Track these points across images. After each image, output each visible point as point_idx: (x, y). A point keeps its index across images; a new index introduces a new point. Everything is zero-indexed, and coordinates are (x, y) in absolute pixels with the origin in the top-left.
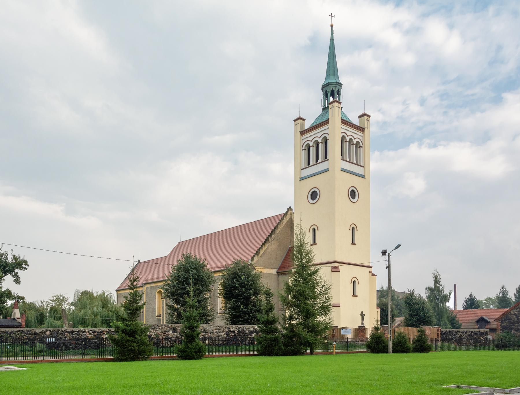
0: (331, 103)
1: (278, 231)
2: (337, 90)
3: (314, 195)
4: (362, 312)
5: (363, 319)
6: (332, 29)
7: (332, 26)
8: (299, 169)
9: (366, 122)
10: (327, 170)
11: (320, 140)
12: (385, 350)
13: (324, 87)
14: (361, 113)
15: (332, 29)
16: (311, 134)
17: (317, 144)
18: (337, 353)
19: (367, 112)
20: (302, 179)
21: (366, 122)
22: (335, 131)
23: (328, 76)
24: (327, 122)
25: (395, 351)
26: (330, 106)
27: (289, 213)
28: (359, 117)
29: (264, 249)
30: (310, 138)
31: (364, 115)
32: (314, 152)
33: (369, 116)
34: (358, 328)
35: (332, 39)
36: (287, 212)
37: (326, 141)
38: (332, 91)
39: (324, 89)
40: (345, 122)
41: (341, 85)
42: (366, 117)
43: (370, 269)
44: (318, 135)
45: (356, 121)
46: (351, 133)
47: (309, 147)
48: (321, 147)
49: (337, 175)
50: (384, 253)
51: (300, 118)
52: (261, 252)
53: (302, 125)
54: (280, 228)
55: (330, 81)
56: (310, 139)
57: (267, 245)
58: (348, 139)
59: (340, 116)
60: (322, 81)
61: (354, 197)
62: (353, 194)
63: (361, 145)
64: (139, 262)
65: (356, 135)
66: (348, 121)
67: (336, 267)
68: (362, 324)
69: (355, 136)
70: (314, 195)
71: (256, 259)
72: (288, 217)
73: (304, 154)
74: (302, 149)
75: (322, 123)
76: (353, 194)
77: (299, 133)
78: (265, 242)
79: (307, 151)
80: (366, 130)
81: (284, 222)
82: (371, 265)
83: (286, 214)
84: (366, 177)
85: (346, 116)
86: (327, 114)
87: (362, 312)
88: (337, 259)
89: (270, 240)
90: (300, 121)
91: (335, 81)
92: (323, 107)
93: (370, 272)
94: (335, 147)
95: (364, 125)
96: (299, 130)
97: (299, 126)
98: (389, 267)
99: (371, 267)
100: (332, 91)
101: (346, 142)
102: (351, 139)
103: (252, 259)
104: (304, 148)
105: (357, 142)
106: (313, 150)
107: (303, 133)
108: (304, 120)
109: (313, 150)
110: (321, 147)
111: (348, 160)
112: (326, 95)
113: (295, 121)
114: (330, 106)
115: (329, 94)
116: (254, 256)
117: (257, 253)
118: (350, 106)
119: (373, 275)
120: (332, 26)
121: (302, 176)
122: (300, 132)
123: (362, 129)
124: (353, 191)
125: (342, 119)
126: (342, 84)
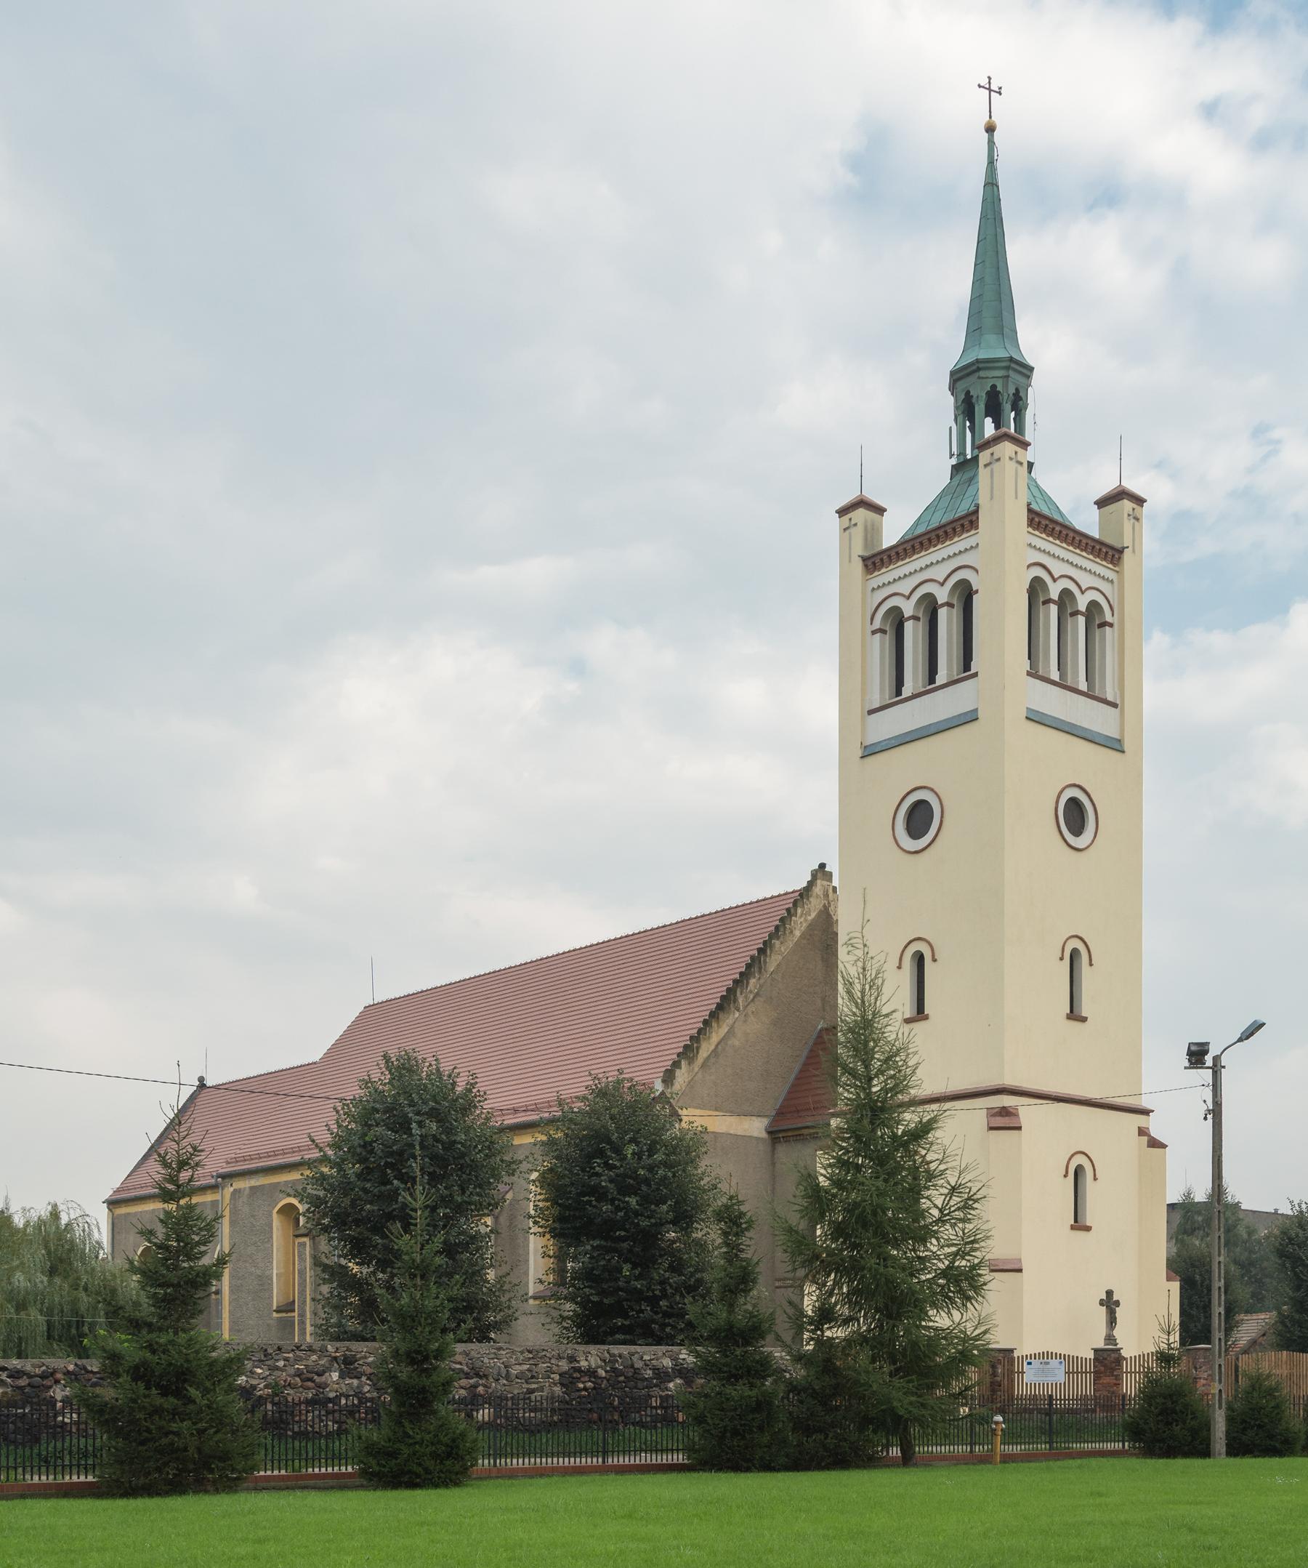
1: (773, 962)
2: (1012, 391)
3: (919, 818)
4: (1110, 1293)
5: (1112, 1321)
6: (991, 143)
7: (990, 129)
9: (1128, 525)
10: (971, 718)
12: (1198, 1447)
13: (958, 377)
14: (1107, 486)
15: (991, 143)
17: (930, 607)
18: (1007, 1459)
20: (870, 751)
21: (1128, 525)
22: (1004, 560)
23: (975, 330)
24: (969, 521)
25: (1237, 1448)
26: (984, 457)
27: (818, 890)
28: (1101, 503)
29: (716, 1035)
30: (904, 584)
31: (1120, 495)
32: (916, 635)
33: (1140, 501)
34: (1091, 1355)
35: (991, 184)
36: (811, 884)
37: (965, 595)
38: (990, 393)
39: (961, 385)
40: (1044, 522)
42: (1127, 505)
43: (1140, 1120)
44: (933, 571)
45: (1088, 521)
47: (897, 621)
48: (947, 622)
50: (1197, 1055)
51: (862, 503)
52: (705, 1049)
53: (872, 533)
54: (782, 949)
56: (905, 587)
57: (730, 1021)
59: (1024, 498)
61: (1077, 829)
62: (1075, 815)
63: (1108, 618)
64: (202, 1085)
67: (1005, 1112)
68: (1110, 1339)
69: (1086, 580)
70: (919, 818)
71: (682, 1076)
72: (814, 905)
73: (879, 648)
74: (870, 628)
75: (951, 524)
76: (1075, 815)
77: (858, 566)
78: (720, 1007)
79: (888, 639)
80: (1127, 555)
81: (799, 925)
82: (1145, 1103)
83: (805, 893)
86: (971, 491)
87: (1110, 1293)
88: (1009, 1081)
89: (741, 1000)
90: (860, 515)
91: (1001, 354)
92: (954, 461)
93: (1142, 1132)
94: (1002, 624)
95: (1122, 534)
96: (858, 549)
97: (858, 534)
98: (1216, 1112)
99: (1146, 1112)
100: (990, 393)
102: (1066, 593)
103: (669, 1077)
104: (877, 624)
105: (1093, 605)
106: (913, 635)
107: (875, 561)
108: (880, 510)
109: (913, 635)
110: (947, 622)
112: (966, 410)
113: (842, 512)
114: (984, 457)
115: (980, 408)
116: (676, 1064)
117: (688, 1052)
119: (1155, 1144)
120: (990, 129)
121: (872, 739)
122: (864, 559)
123: (1110, 553)
124: (1074, 802)
125: (1030, 511)
126: (1031, 369)
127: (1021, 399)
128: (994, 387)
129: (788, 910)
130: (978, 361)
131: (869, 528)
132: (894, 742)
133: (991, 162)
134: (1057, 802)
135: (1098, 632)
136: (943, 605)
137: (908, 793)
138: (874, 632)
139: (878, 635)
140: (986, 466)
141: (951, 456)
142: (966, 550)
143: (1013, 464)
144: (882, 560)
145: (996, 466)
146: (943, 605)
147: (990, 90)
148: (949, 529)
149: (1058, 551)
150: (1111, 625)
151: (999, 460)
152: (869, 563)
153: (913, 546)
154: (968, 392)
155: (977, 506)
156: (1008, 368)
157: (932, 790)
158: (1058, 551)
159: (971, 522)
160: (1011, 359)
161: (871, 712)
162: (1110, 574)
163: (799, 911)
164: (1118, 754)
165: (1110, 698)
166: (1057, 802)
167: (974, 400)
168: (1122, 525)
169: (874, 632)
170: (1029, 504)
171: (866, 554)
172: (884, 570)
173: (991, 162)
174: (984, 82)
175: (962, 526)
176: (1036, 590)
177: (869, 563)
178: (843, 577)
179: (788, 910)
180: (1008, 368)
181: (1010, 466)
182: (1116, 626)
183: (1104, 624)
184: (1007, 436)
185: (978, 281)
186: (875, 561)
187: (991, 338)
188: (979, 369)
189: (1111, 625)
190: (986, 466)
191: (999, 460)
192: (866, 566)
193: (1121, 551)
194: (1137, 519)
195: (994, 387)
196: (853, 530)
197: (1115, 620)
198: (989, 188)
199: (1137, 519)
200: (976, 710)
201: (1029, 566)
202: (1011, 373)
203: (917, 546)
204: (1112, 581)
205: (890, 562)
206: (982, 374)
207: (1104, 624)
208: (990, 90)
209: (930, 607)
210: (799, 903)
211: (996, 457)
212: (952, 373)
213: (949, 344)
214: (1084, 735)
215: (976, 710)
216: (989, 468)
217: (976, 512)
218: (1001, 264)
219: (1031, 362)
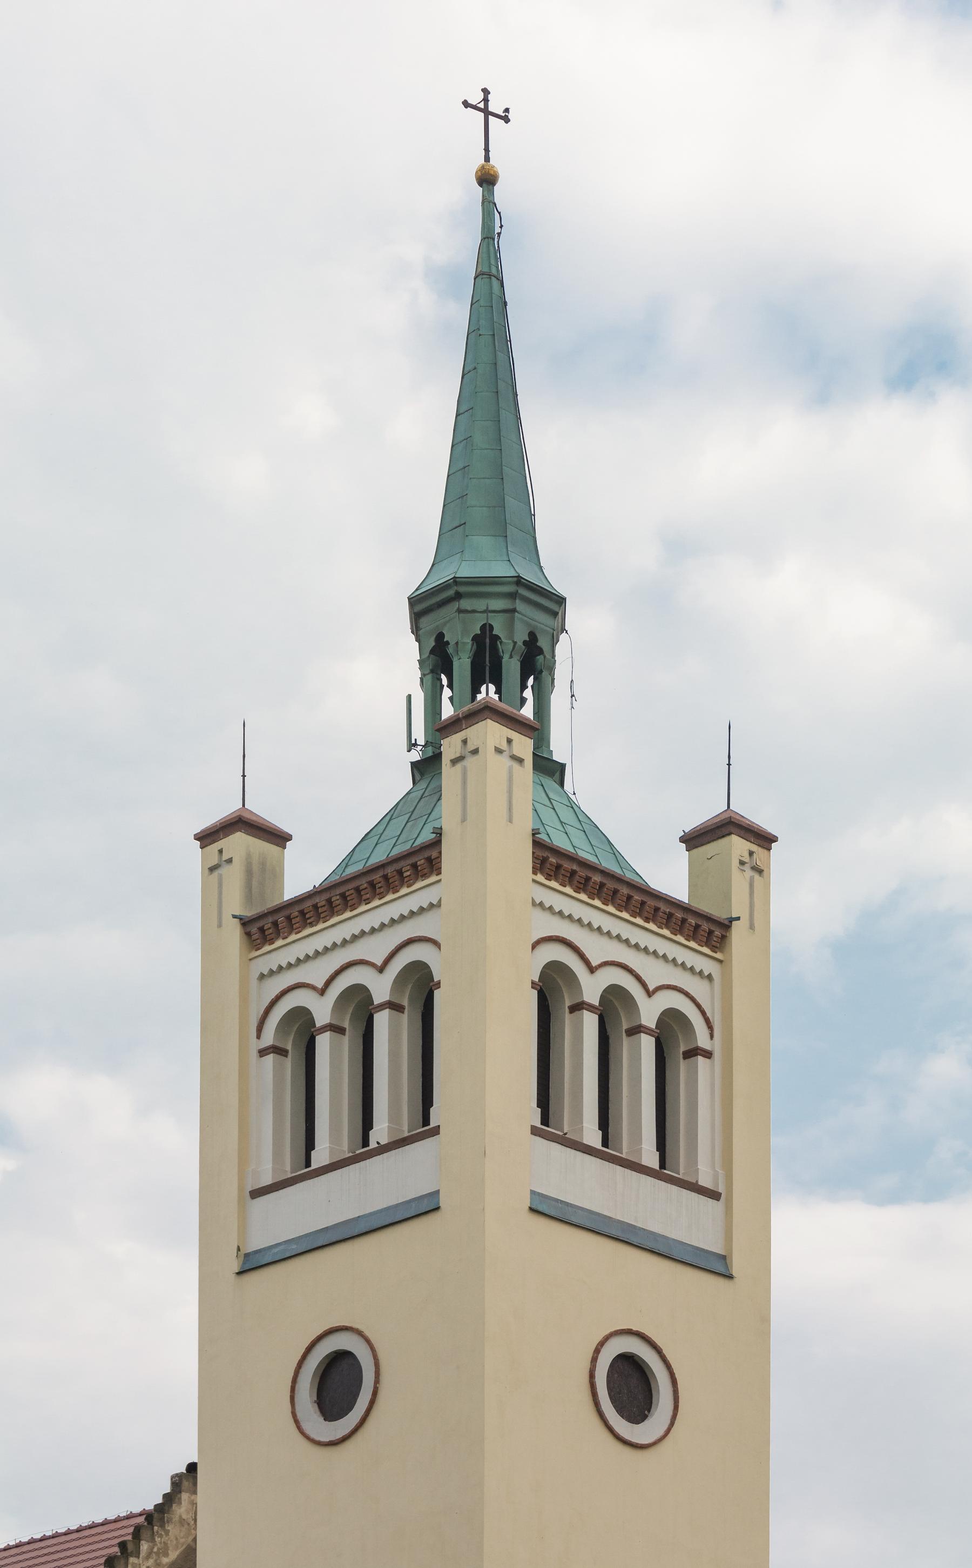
0: (454, 725)
2: (521, 636)
3: (337, 1383)
6: (489, 205)
7: (487, 179)
8: (231, 1191)
9: (740, 881)
10: (427, 1207)
11: (381, 988)
13: (423, 607)
14: (707, 810)
15: (489, 205)
16: (319, 942)
17: (359, 1006)
19: (750, 809)
20: (252, 1264)
21: (740, 881)
22: (491, 933)
23: (455, 527)
24: (422, 861)
26: (450, 746)
28: (693, 840)
31: (726, 826)
33: (765, 840)
36: (169, 1499)
37: (420, 989)
38: (487, 638)
39: (427, 623)
41: (553, 604)
42: (738, 845)
44: (366, 944)
45: (669, 873)
46: (609, 948)
49: (504, 1243)
51: (241, 823)
53: (263, 875)
55: (466, 571)
56: (317, 973)
58: (592, 988)
59: (525, 823)
60: (413, 561)
62: (631, 1385)
63: (702, 1040)
65: (660, 972)
66: (629, 875)
70: (337, 1383)
72: (173, 1533)
74: (255, 1045)
75: (400, 864)
76: (631, 1385)
77: (234, 932)
80: (738, 933)
83: (155, 1518)
84: (737, 1267)
85: (589, 828)
90: (238, 842)
91: (500, 570)
92: (415, 756)
95: (727, 897)
96: (235, 904)
97: (234, 877)
100: (487, 638)
101: (578, 1007)
102: (614, 994)
104: (269, 1038)
105: (671, 1018)
107: (268, 925)
108: (280, 838)
111: (593, 1137)
112: (437, 661)
113: (206, 838)
114: (450, 746)
115: (511, 667)
118: (625, 753)
120: (487, 179)
121: (256, 1243)
122: (245, 923)
123: (705, 928)
124: (627, 1362)
125: (537, 844)
126: (561, 601)
127: (540, 651)
128: (487, 628)
129: (123, 1545)
130: (456, 581)
131: (255, 868)
132: (295, 1248)
133: (489, 238)
134: (594, 1360)
135: (683, 1065)
136: (382, 1007)
137: (597, 1351)
138: (263, 1053)
139: (270, 1058)
140: (454, 762)
141: (412, 745)
142: (335, 945)
143: (505, 761)
144: (275, 924)
145: (470, 762)
146: (382, 1007)
147: (487, 113)
148: (336, 900)
149: (598, 919)
150: (708, 1054)
151: (475, 752)
152: (254, 929)
153: (329, 901)
154: (440, 636)
155: (439, 832)
156: (513, 596)
157: (359, 1333)
158: (598, 919)
159: (429, 860)
160: (519, 581)
161: (257, 1193)
162: (707, 966)
163: (144, 1546)
164: (721, 1282)
165: (705, 1181)
166: (594, 1360)
167: (450, 650)
168: (729, 880)
169: (263, 1053)
170: (535, 833)
171: (248, 913)
172: (280, 942)
173: (489, 238)
174: (476, 98)
175: (414, 866)
176: (551, 992)
177: (254, 929)
178: (209, 951)
179: (123, 1545)
180: (513, 596)
181: (498, 766)
182: (717, 1055)
183: (693, 1052)
184: (488, 711)
185: (462, 443)
186: (268, 925)
187: (483, 542)
188: (458, 596)
189: (708, 1054)
190: (454, 762)
191: (475, 752)
192: (248, 934)
193: (726, 925)
194: (760, 872)
195: (487, 628)
196: (225, 870)
197: (716, 1046)
198: (482, 282)
199: (760, 872)
200: (438, 1192)
201: (534, 946)
202: (520, 606)
203: (336, 900)
204: (710, 977)
205: (291, 929)
206: (465, 604)
207: (693, 1052)
208: (487, 113)
209: (359, 1006)
210: (145, 1534)
211: (471, 747)
212: (413, 601)
213: (404, 543)
214: (650, 1245)
215: (438, 1192)
216: (459, 766)
217: (436, 843)
218: (505, 415)
219: (560, 588)
